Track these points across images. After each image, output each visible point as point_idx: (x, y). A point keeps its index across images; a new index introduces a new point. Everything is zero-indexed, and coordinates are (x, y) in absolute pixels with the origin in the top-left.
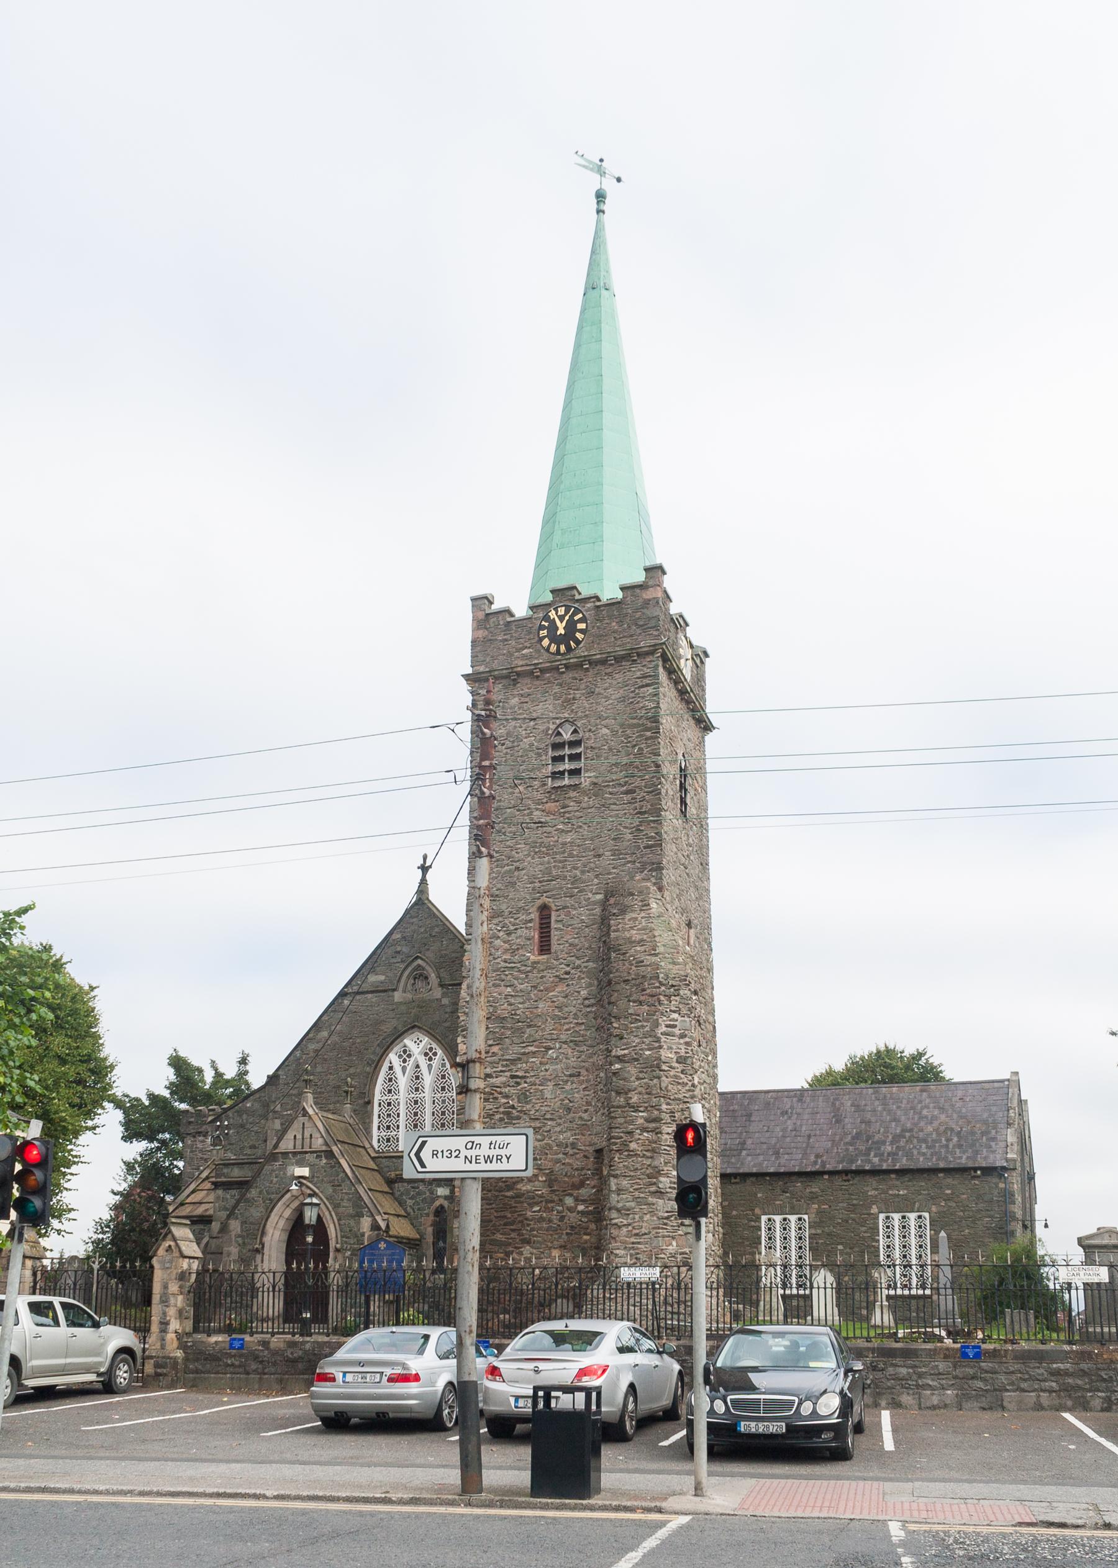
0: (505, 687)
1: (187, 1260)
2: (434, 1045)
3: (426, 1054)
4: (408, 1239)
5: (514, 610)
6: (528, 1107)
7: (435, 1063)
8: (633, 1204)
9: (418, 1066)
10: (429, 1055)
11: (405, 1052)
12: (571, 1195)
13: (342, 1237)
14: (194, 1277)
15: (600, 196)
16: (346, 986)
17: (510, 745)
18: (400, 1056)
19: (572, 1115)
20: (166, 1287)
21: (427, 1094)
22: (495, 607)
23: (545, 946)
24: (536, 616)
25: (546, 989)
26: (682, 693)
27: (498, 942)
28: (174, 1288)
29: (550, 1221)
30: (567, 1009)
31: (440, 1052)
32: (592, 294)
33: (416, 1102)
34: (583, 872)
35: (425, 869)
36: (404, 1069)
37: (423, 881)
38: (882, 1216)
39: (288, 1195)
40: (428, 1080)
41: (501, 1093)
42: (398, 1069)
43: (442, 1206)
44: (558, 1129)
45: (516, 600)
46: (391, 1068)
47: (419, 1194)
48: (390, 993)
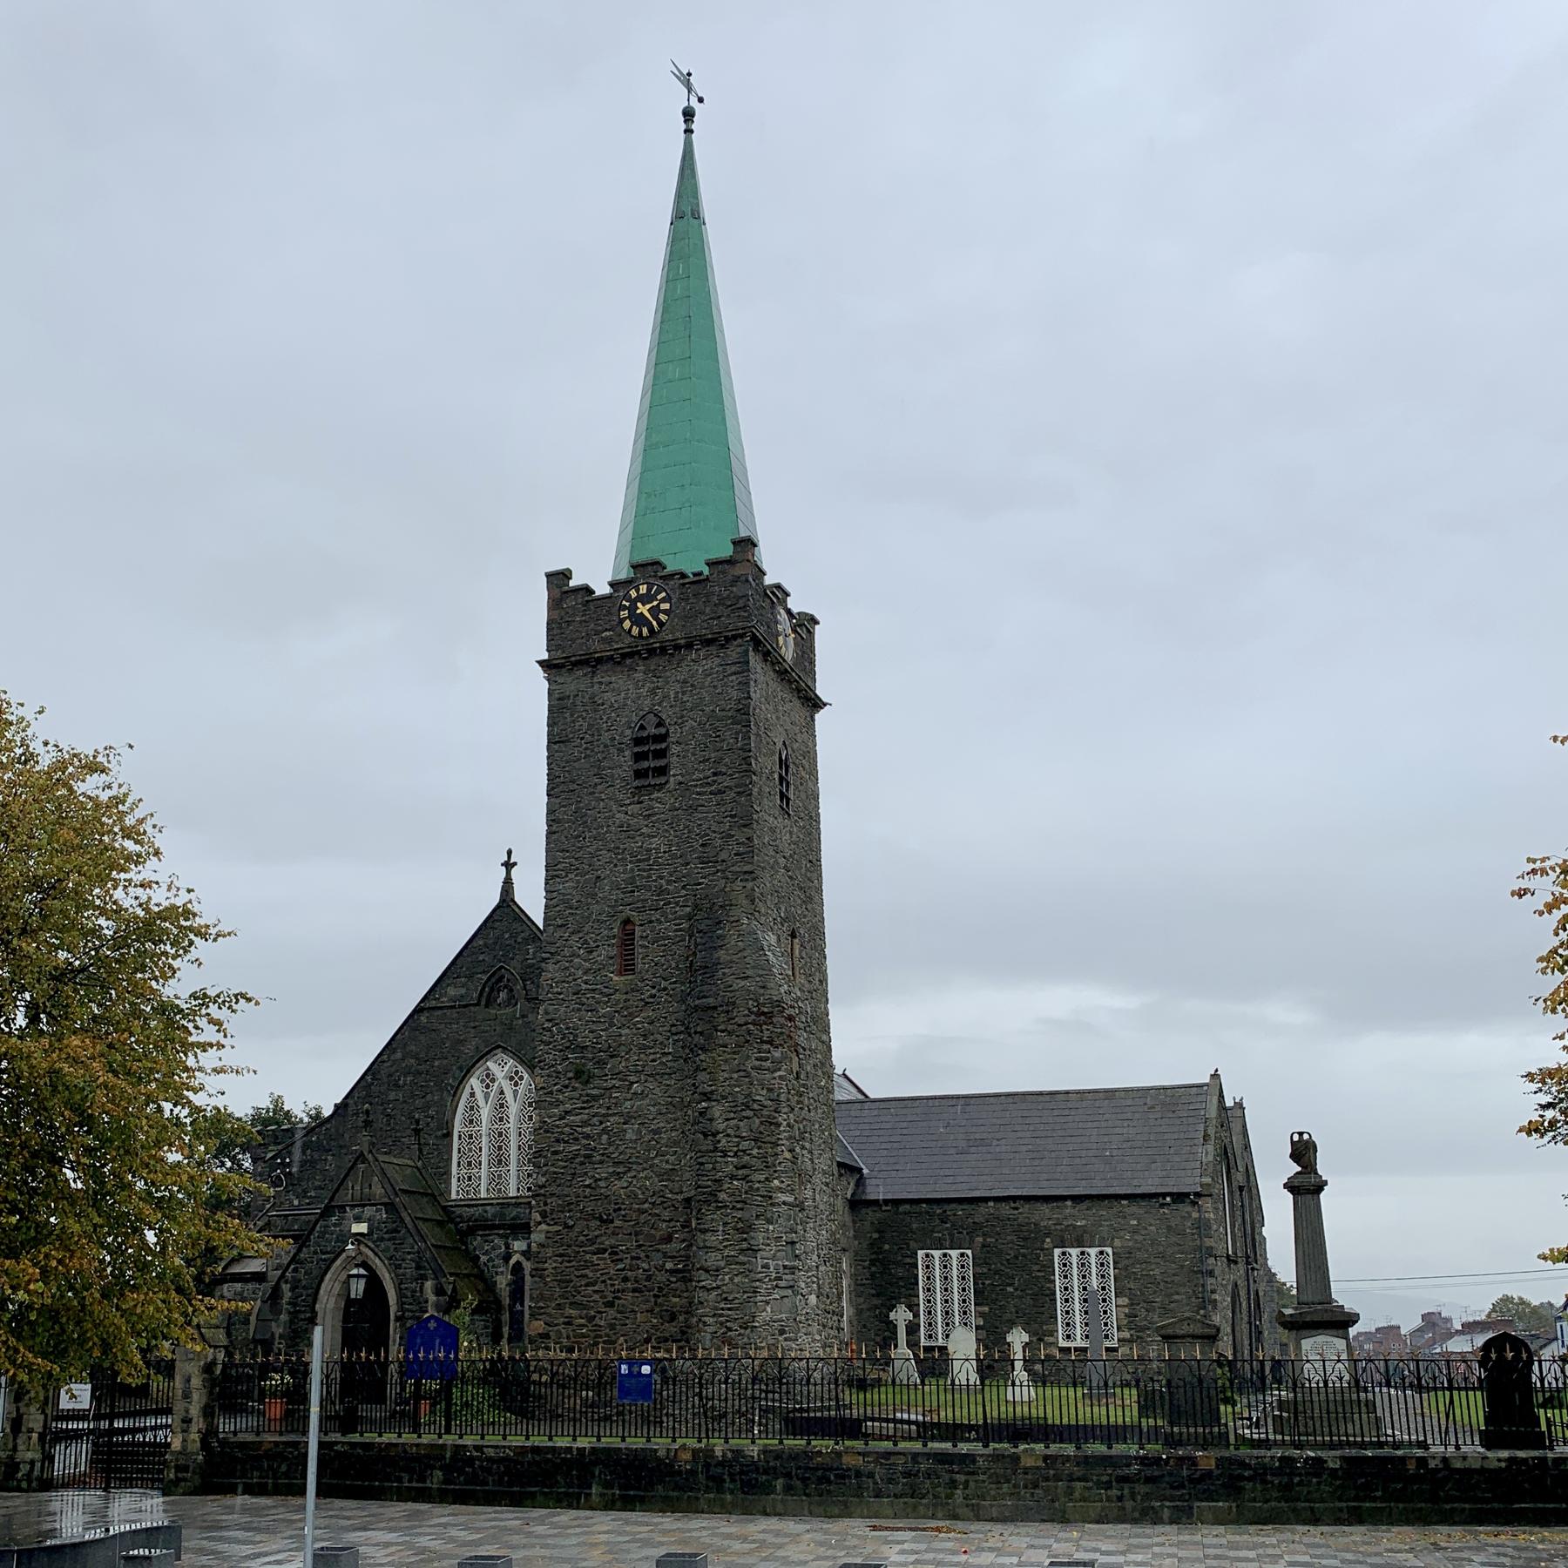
2: (520, 1068)
3: (511, 1079)
6: (611, 1149)
7: (521, 1088)
8: (722, 1263)
9: (502, 1092)
10: (514, 1078)
11: (488, 1076)
14: (220, 1367)
15: (688, 114)
16: (423, 1000)
18: (482, 1081)
21: (512, 1125)
22: (572, 583)
23: (627, 968)
25: (630, 1014)
26: (783, 674)
31: (526, 1076)
34: (669, 883)
35: (509, 866)
37: (508, 884)
38: (1057, 1252)
39: (344, 1255)
40: (513, 1109)
42: (479, 1095)
43: (518, 1263)
45: (597, 573)
46: (472, 1095)
47: (493, 1249)
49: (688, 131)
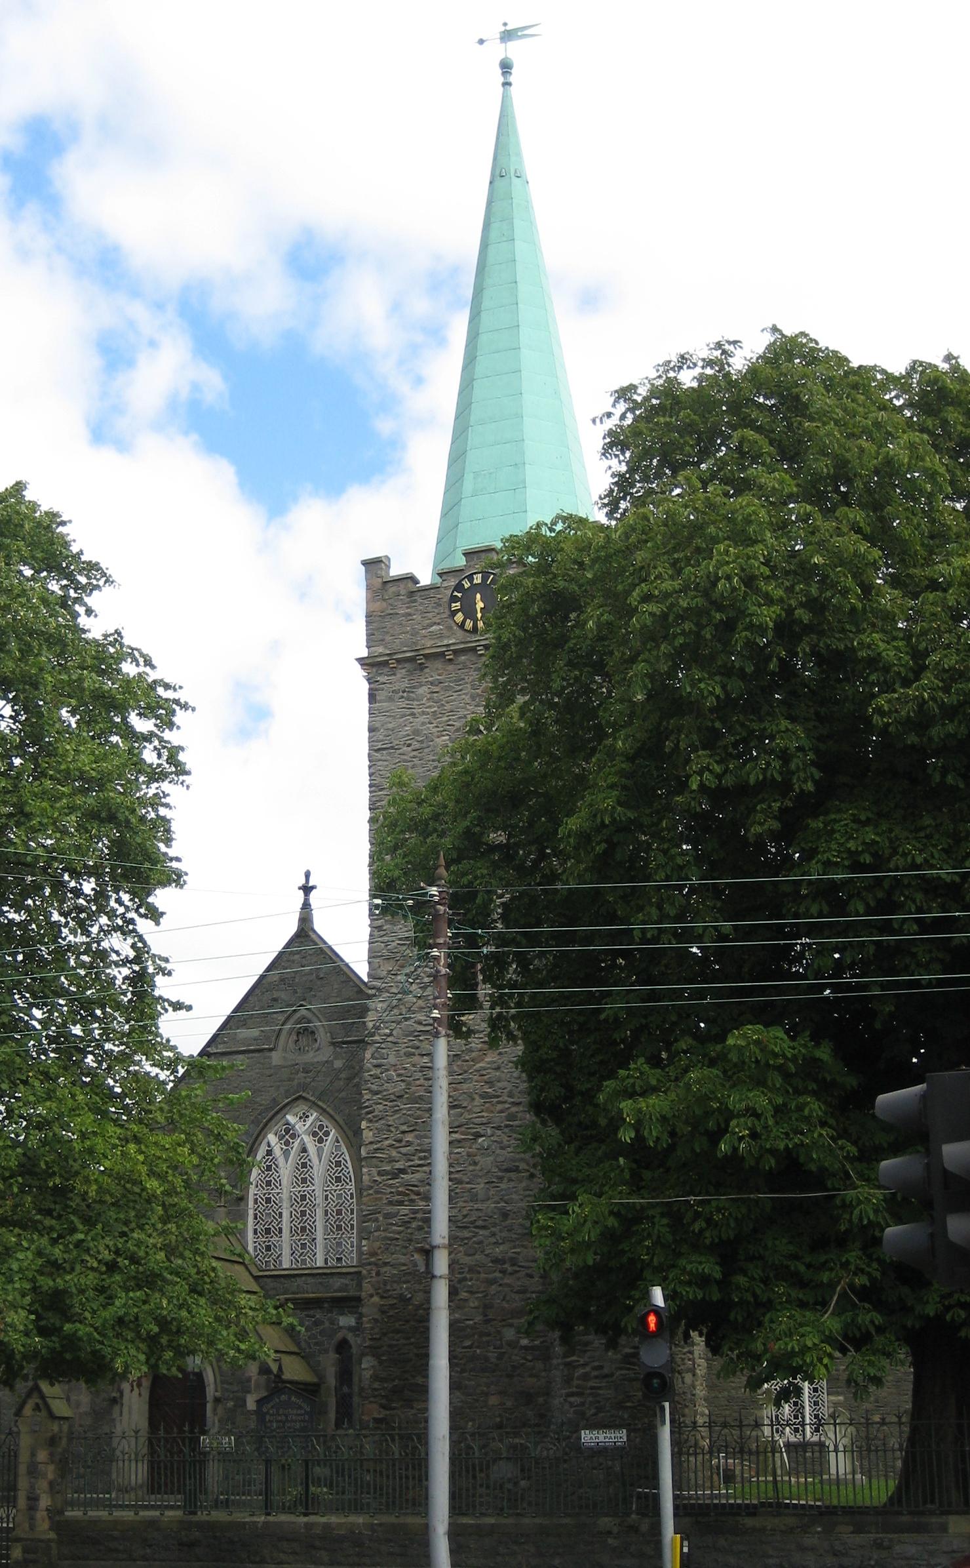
0: (410, 673)
1: (57, 1422)
2: (325, 1122)
3: (315, 1134)
4: (306, 1384)
5: (418, 576)
9: (304, 1150)
10: (319, 1135)
12: (511, 1325)
13: (222, 1382)
15: (506, 67)
16: (209, 1044)
17: (418, 746)
19: (509, 1222)
20: (33, 1455)
21: (317, 1188)
24: (445, 584)
27: (410, 998)
28: (42, 1456)
29: (487, 1359)
30: (499, 1084)
32: (499, 183)
33: (303, 1198)
35: (307, 889)
36: (286, 1154)
37: (306, 906)
40: (318, 1169)
41: (418, 1194)
42: (277, 1152)
44: (493, 1240)
45: (418, 562)
46: (269, 1153)
48: (268, 1054)
49: (507, 84)
